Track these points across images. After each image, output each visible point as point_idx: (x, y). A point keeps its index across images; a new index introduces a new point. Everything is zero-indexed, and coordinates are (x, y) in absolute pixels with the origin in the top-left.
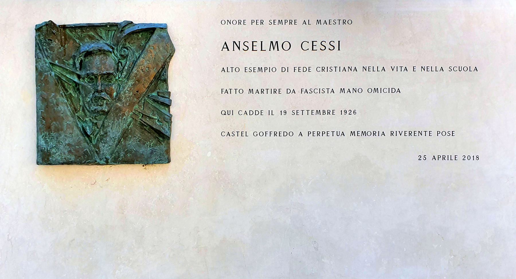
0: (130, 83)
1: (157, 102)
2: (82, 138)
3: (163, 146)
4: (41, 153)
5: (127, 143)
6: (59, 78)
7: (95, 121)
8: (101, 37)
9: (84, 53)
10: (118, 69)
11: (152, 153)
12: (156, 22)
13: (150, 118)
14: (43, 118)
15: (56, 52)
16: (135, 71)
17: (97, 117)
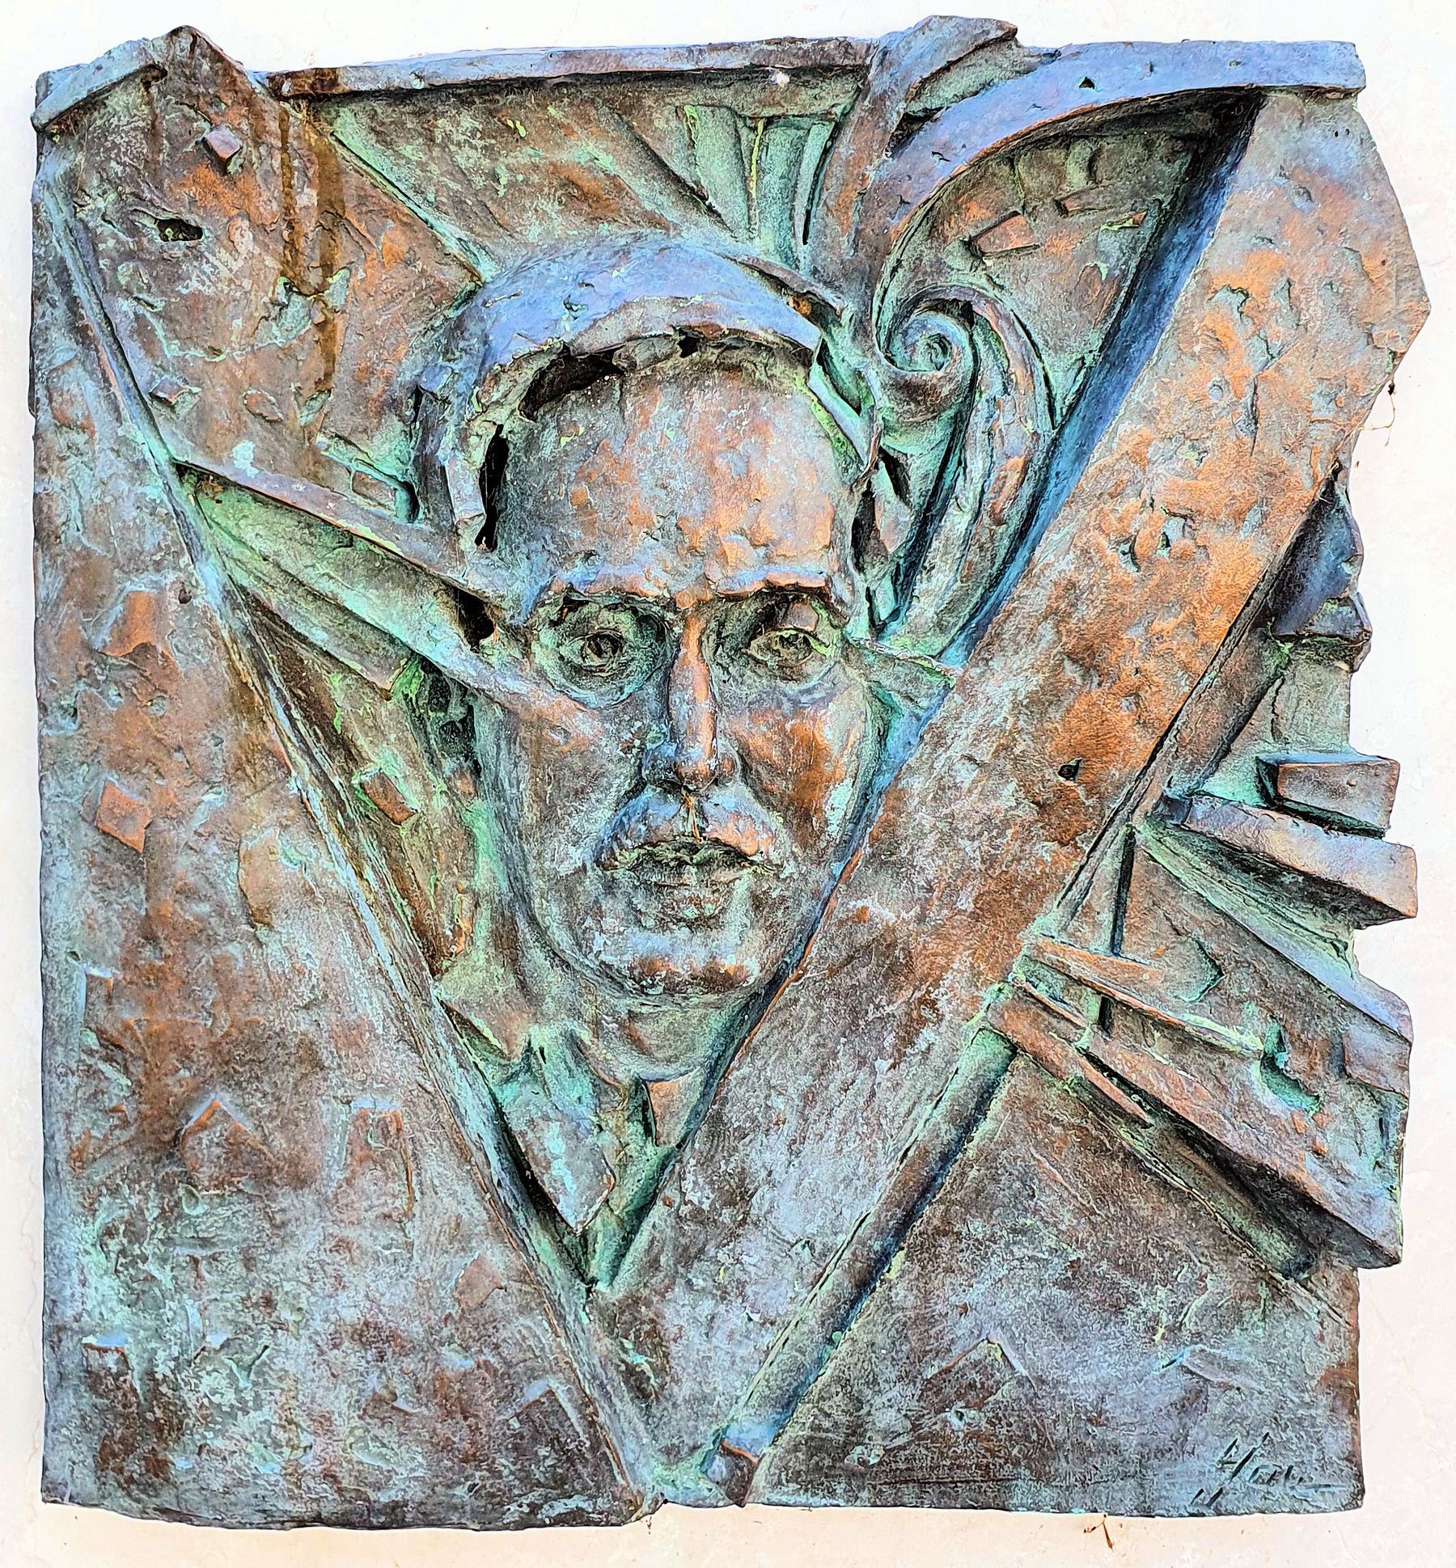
0: (1008, 679)
1: (1268, 873)
2: (497, 1258)
3: (1299, 1333)
4: (88, 1399)
5: (948, 1292)
6: (271, 625)
7: (626, 1067)
8: (694, 196)
9: (528, 374)
10: (863, 531)
11: (1192, 1402)
12: (1250, 33)
13: (1182, 1039)
14: (112, 1047)
15: (234, 352)
16: (1055, 554)
17: (644, 1030)
